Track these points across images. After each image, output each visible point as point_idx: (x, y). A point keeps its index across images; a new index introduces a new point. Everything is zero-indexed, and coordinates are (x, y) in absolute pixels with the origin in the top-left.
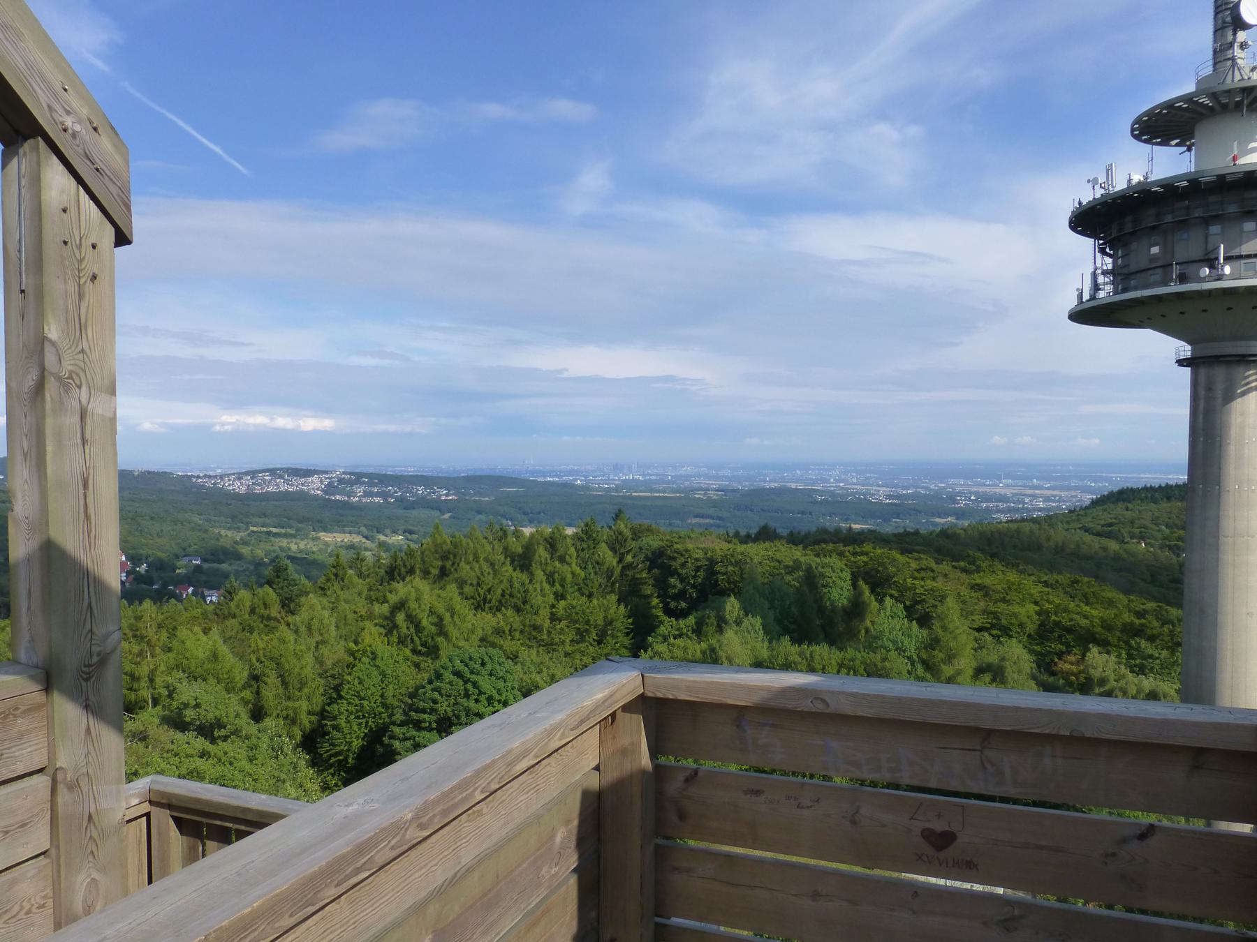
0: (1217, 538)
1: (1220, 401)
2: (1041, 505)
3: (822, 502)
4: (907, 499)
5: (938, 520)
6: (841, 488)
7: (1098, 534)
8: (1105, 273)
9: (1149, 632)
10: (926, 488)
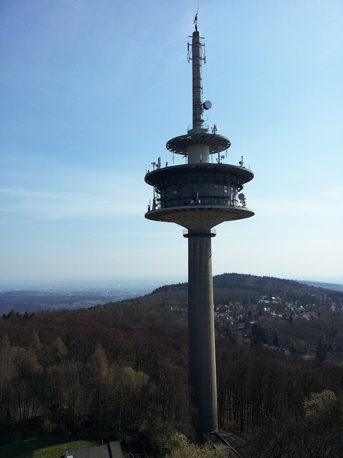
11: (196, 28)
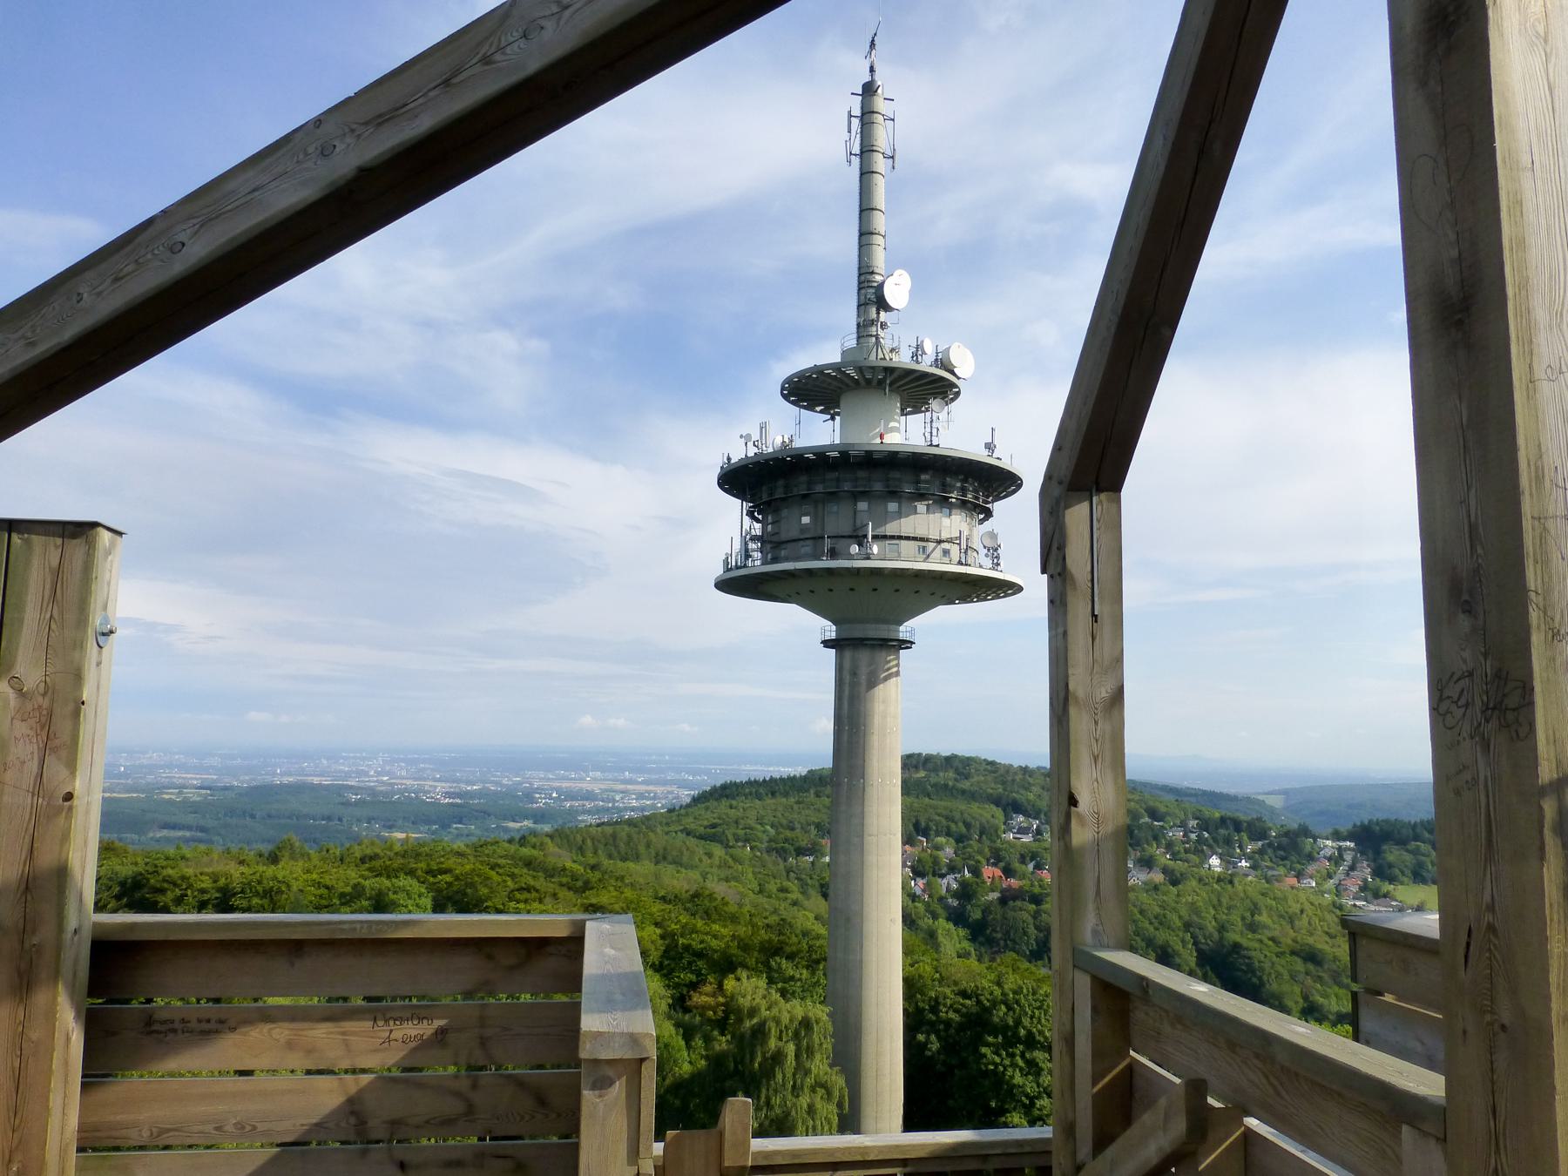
0: (862, 837)
1: (863, 688)
2: (634, 803)
3: (357, 803)
4: (472, 798)
5: (511, 825)
6: (383, 782)
7: (701, 837)
8: (754, 538)
9: (788, 949)
10: (496, 783)
11: (872, 70)
